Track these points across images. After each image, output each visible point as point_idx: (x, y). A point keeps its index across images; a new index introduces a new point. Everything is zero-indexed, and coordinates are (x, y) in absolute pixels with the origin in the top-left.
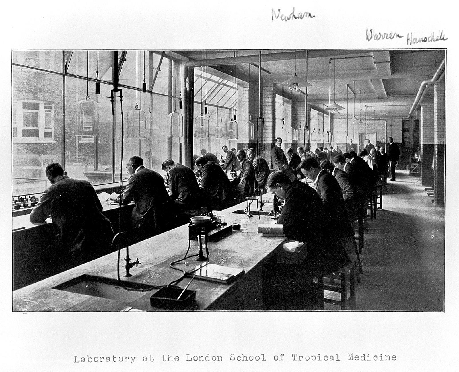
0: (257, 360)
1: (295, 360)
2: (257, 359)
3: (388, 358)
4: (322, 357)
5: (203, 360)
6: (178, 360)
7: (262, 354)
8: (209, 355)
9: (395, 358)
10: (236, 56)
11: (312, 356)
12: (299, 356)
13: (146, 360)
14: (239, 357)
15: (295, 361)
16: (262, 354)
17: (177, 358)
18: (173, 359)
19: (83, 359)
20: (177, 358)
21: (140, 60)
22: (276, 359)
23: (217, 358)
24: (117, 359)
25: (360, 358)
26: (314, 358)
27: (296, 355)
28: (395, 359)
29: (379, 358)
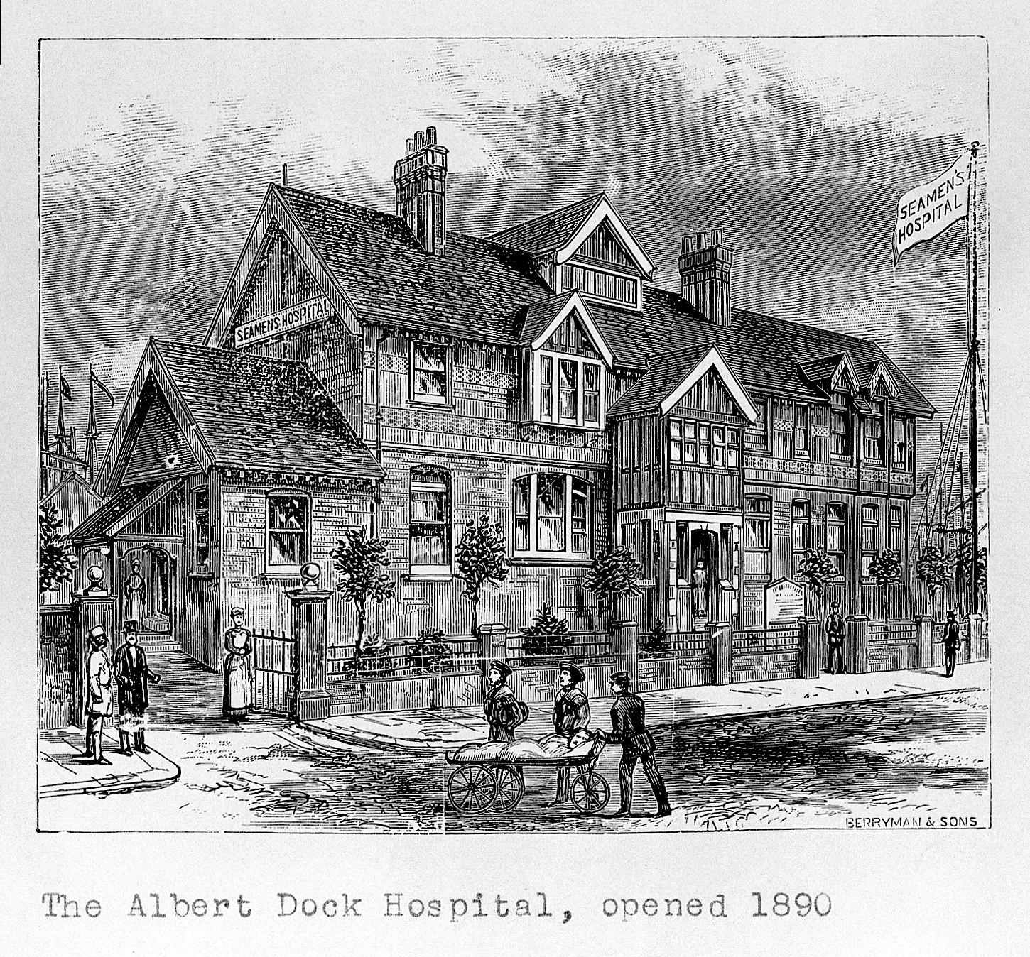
0: (310, 914)
1: (399, 914)
2: (307, 911)
3: (675, 906)
4: (489, 905)
5: (680, 914)
6: (700, 911)
7: (754, 894)
8: (723, 896)
9: (97, 911)
10: (832, 456)
11: (454, 902)
12: (216, 901)
13: (525, 910)
14: (331, 904)
15: (388, 916)
16: (754, 894)
17: (93, 908)
18: (82, 911)
19: (522, 904)
20: (352, 906)
21: (425, 324)
22: (307, 911)
23: (621, 905)
24: (512, 906)
25: (705, 908)
26: (459, 907)
27: (55, 898)
28: (653, 910)
29: (473, 908)
